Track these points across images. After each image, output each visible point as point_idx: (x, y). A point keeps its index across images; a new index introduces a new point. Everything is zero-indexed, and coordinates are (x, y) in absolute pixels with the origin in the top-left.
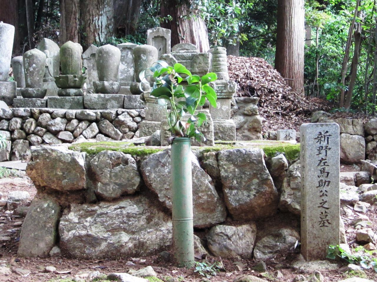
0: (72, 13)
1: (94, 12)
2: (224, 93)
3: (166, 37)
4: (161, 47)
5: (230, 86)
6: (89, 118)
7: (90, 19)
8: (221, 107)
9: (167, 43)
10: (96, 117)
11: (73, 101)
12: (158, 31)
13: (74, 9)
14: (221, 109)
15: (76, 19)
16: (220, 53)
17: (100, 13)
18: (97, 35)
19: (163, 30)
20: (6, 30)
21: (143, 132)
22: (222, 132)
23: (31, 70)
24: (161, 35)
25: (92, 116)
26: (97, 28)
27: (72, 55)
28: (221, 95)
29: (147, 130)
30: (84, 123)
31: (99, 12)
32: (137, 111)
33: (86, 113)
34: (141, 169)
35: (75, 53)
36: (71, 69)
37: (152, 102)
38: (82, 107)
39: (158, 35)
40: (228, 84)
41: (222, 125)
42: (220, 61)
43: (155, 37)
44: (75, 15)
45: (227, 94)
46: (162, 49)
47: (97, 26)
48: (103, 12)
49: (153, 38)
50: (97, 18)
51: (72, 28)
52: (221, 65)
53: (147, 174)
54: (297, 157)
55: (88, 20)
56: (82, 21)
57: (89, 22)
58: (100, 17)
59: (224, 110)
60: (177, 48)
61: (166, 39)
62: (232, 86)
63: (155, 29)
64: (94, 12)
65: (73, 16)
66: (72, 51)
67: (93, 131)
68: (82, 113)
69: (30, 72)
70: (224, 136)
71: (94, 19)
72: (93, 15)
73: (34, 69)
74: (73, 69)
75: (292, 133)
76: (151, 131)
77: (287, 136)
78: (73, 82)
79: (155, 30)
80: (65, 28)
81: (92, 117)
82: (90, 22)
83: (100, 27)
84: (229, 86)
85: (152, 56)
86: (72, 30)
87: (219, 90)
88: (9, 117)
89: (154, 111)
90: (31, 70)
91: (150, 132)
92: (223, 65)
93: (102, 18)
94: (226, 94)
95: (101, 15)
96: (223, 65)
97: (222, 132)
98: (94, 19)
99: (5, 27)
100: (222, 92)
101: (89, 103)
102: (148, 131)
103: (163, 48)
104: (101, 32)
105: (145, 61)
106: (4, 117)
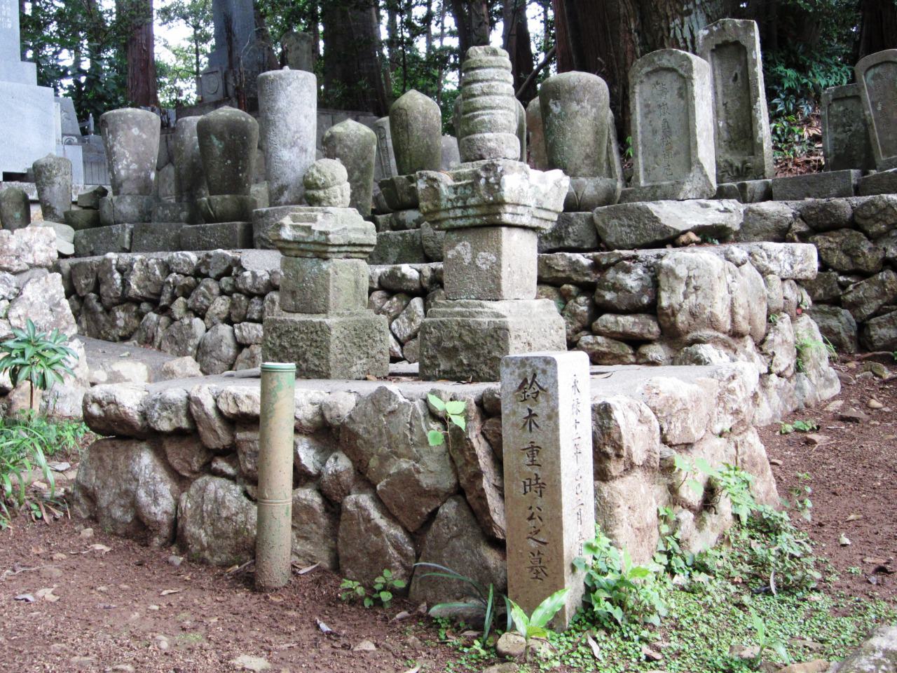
0: (619, 19)
1: (668, 8)
2: (472, 206)
3: (743, 43)
4: (738, 70)
5: (487, 179)
6: (405, 285)
7: (661, 28)
8: (474, 257)
9: (748, 57)
10: (421, 282)
11: (402, 242)
12: (723, 29)
13: (622, 11)
14: (473, 263)
15: (631, 33)
16: (473, 69)
17: (685, 8)
19: (735, 25)
20: (284, 84)
21: (270, 349)
22: (468, 347)
24: (731, 39)
25: (410, 280)
27: (407, 126)
28: (468, 217)
29: (278, 342)
30: (395, 299)
31: (682, 7)
32: (588, 257)
33: (399, 275)
35: (416, 118)
36: (408, 161)
37: (293, 253)
39: (724, 39)
40: (483, 174)
41: (471, 320)
42: (474, 96)
43: (717, 46)
44: (627, 23)
45: (485, 210)
46: (739, 76)
48: (691, 6)
49: (713, 51)
50: (677, 21)
51: (625, 55)
52: (478, 109)
55: (657, 31)
56: (648, 35)
57: (660, 34)
58: (686, 19)
59: (484, 267)
60: (642, 67)
61: (744, 48)
62: (492, 180)
63: (716, 25)
64: (668, 8)
65: (622, 26)
66: (407, 115)
67: (411, 320)
68: (392, 275)
70: (474, 360)
72: (667, 17)
74: (414, 159)
75: (544, 372)
76: (286, 344)
77: (525, 381)
78: (409, 194)
79: (715, 29)
81: (410, 284)
82: (663, 35)
83: (689, 44)
84: (482, 181)
85: (578, 102)
86: (625, 60)
87: (457, 199)
88: (263, 291)
89: (297, 281)
91: (285, 348)
92: (484, 108)
93: (691, 21)
94: (479, 212)
95: (689, 13)
96: (484, 108)
97: (468, 347)
98: (672, 26)
99: (281, 77)
100: (465, 207)
101: (431, 244)
102: (280, 345)
103: (742, 74)
105: (559, 116)
106: (255, 291)
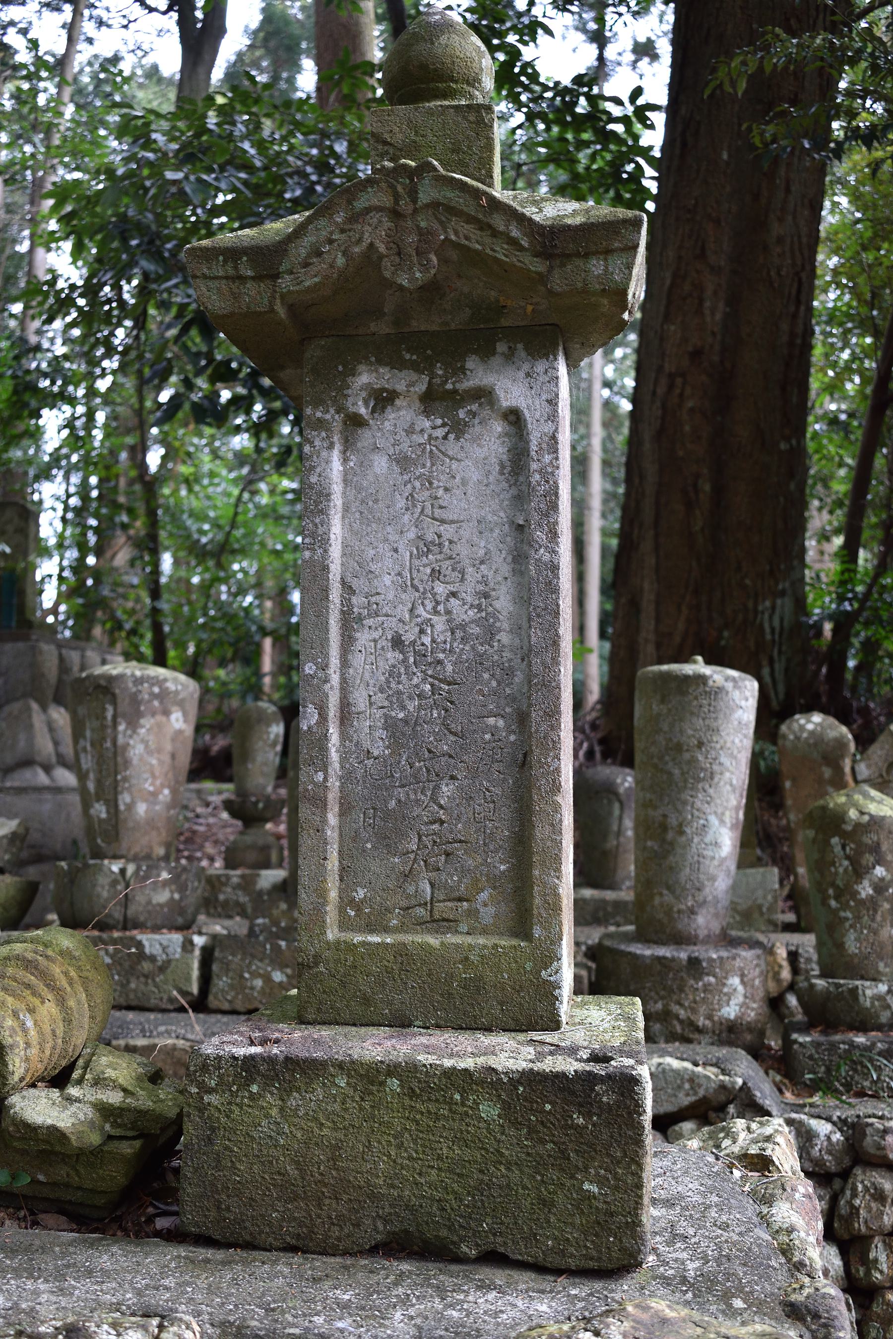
17: (780, 587)
18: (765, 662)
23: (863, 895)
26: (768, 637)
31: (777, 584)
34: (512, 430)
38: (668, 1108)
47: (768, 630)
50: (768, 603)
53: (509, 539)
54: (464, 1291)
58: (779, 602)
69: (862, 902)
71: (760, 608)
73: (880, 887)
80: (652, 637)
83: (777, 637)
90: (863, 895)
95: (783, 593)
104: (780, 652)
